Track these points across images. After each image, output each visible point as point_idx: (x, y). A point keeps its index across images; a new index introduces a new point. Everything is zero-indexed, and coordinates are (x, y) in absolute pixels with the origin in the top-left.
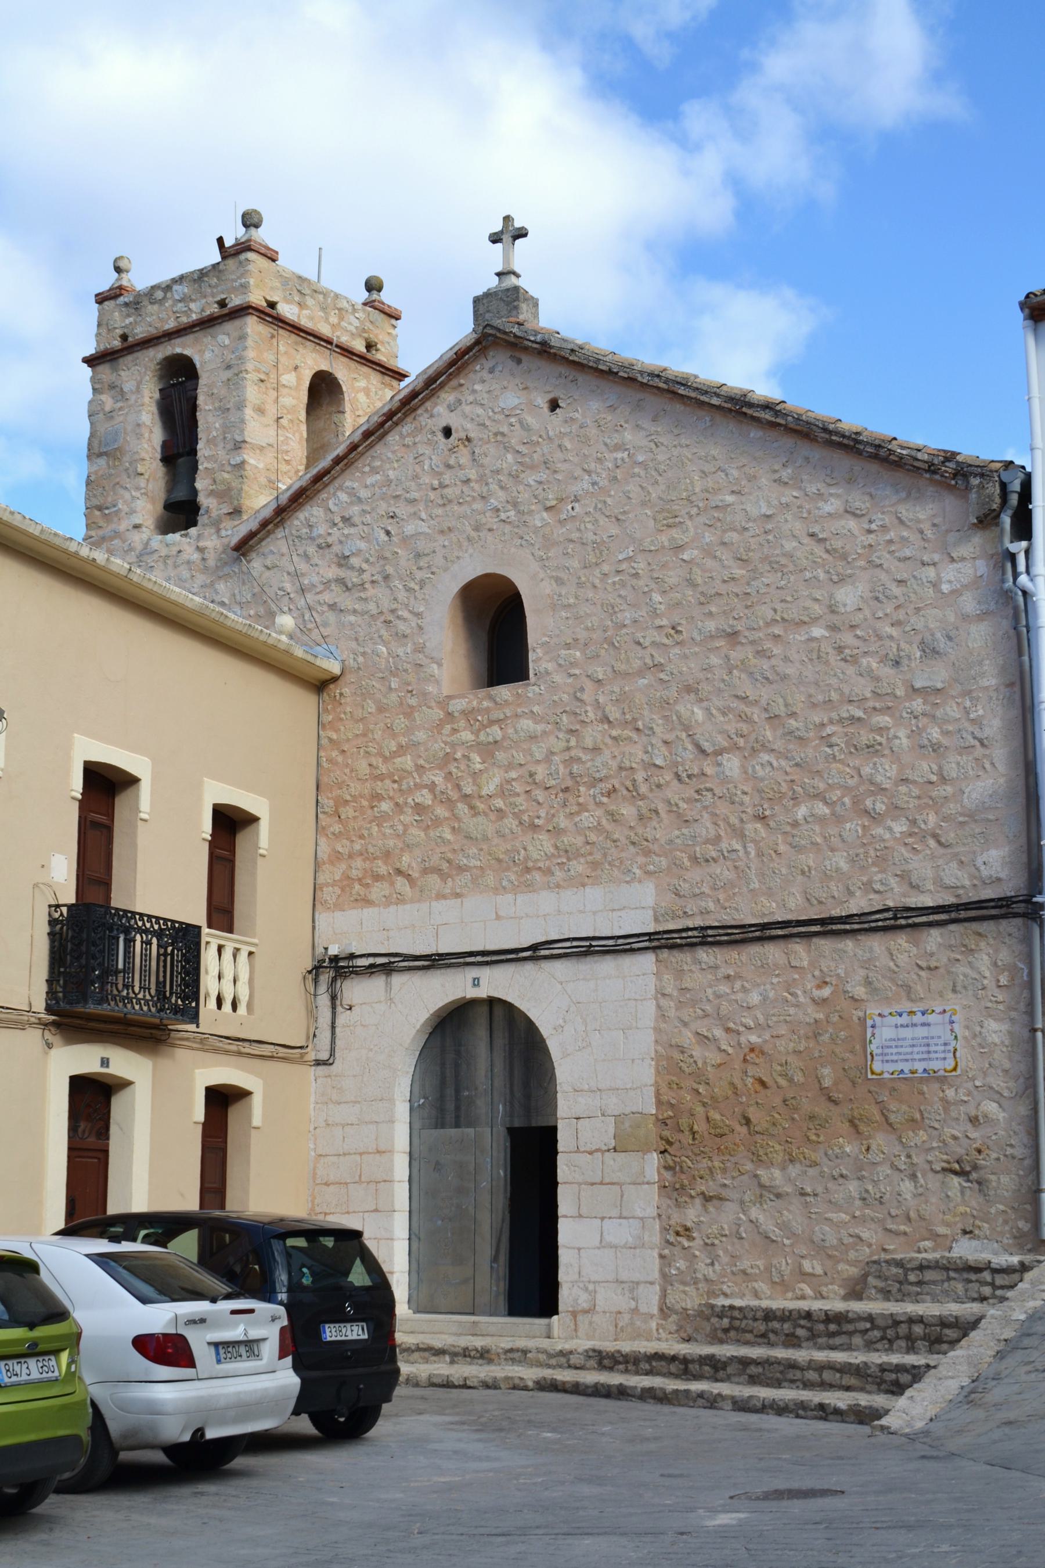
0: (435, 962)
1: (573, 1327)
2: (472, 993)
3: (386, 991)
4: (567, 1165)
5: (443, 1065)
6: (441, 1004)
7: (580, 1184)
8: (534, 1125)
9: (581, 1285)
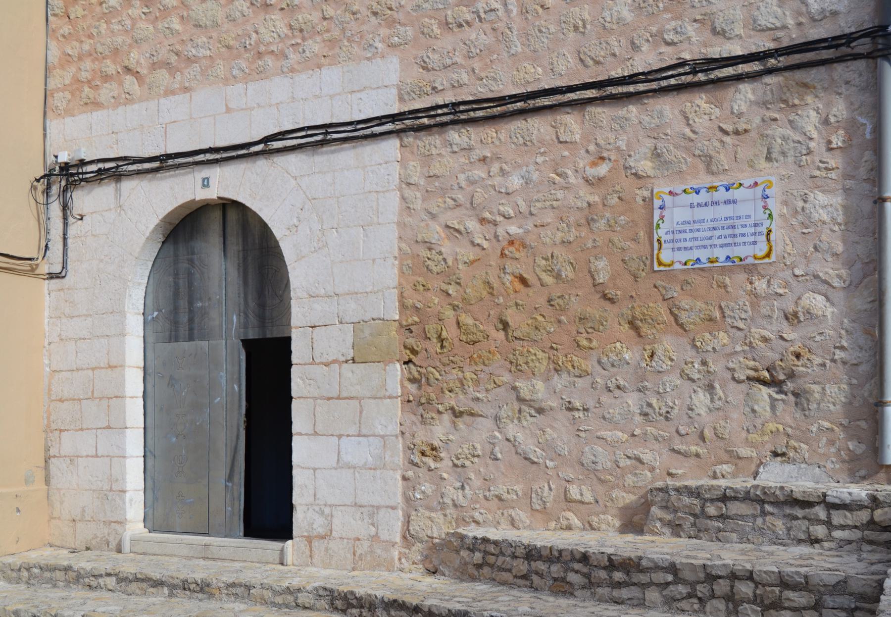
0: (164, 163)
1: (308, 553)
3: (116, 197)
5: (176, 275)
7: (315, 399)
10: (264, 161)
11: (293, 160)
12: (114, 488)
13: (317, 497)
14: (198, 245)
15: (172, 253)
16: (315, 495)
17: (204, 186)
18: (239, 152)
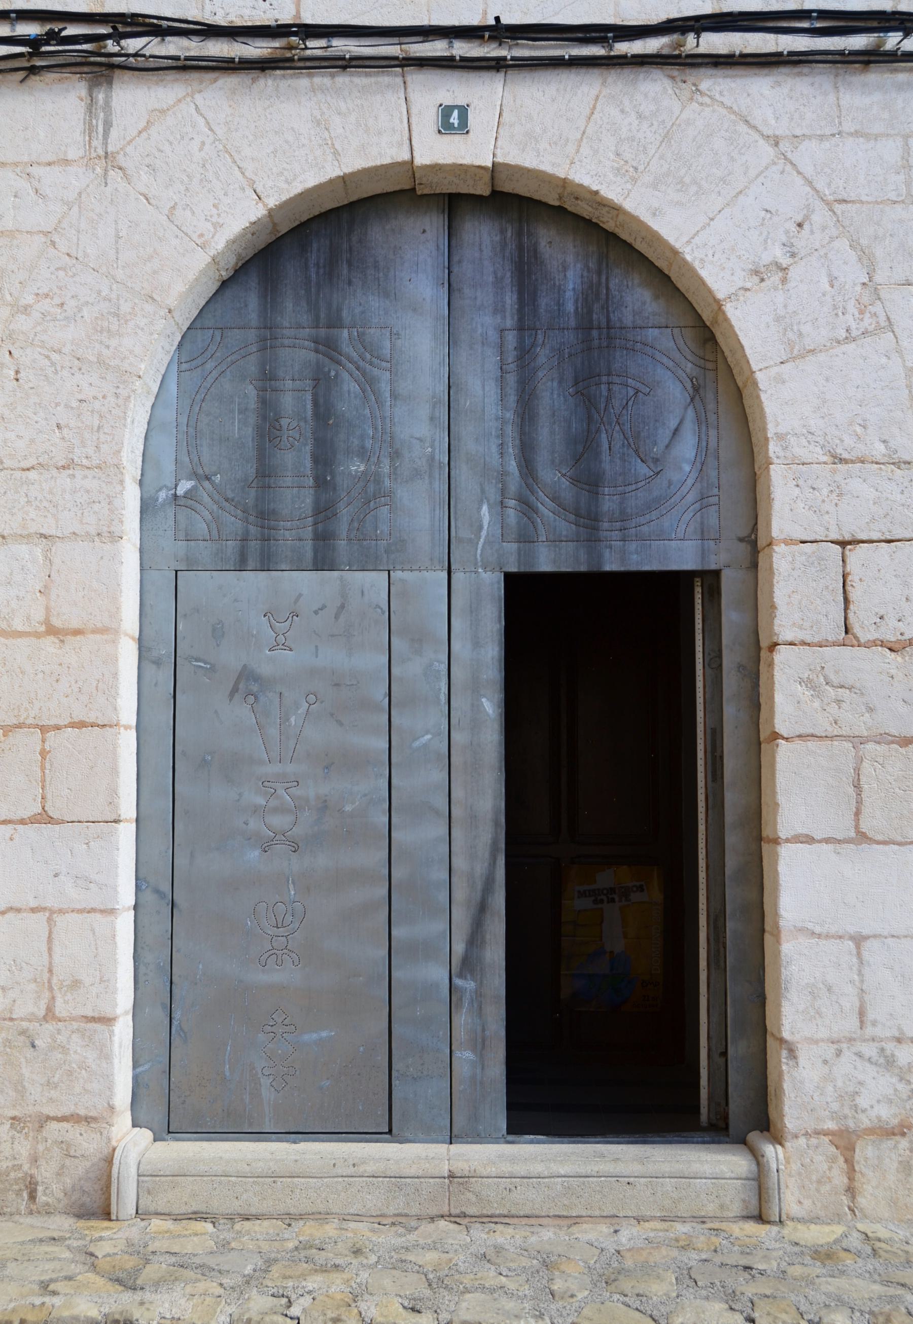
0: (291, 50)
1: (840, 1180)
2: (434, 150)
3: (90, 130)
4: (808, 683)
5: (268, 379)
6: (311, 180)
7: (858, 741)
8: (611, 564)
9: (870, 1050)
10: (667, 83)
11: (766, 91)
12: (61, 1009)
13: (871, 1015)
14: (360, 302)
15: (253, 317)
16: (862, 1014)
17: (445, 127)
18: (596, 47)
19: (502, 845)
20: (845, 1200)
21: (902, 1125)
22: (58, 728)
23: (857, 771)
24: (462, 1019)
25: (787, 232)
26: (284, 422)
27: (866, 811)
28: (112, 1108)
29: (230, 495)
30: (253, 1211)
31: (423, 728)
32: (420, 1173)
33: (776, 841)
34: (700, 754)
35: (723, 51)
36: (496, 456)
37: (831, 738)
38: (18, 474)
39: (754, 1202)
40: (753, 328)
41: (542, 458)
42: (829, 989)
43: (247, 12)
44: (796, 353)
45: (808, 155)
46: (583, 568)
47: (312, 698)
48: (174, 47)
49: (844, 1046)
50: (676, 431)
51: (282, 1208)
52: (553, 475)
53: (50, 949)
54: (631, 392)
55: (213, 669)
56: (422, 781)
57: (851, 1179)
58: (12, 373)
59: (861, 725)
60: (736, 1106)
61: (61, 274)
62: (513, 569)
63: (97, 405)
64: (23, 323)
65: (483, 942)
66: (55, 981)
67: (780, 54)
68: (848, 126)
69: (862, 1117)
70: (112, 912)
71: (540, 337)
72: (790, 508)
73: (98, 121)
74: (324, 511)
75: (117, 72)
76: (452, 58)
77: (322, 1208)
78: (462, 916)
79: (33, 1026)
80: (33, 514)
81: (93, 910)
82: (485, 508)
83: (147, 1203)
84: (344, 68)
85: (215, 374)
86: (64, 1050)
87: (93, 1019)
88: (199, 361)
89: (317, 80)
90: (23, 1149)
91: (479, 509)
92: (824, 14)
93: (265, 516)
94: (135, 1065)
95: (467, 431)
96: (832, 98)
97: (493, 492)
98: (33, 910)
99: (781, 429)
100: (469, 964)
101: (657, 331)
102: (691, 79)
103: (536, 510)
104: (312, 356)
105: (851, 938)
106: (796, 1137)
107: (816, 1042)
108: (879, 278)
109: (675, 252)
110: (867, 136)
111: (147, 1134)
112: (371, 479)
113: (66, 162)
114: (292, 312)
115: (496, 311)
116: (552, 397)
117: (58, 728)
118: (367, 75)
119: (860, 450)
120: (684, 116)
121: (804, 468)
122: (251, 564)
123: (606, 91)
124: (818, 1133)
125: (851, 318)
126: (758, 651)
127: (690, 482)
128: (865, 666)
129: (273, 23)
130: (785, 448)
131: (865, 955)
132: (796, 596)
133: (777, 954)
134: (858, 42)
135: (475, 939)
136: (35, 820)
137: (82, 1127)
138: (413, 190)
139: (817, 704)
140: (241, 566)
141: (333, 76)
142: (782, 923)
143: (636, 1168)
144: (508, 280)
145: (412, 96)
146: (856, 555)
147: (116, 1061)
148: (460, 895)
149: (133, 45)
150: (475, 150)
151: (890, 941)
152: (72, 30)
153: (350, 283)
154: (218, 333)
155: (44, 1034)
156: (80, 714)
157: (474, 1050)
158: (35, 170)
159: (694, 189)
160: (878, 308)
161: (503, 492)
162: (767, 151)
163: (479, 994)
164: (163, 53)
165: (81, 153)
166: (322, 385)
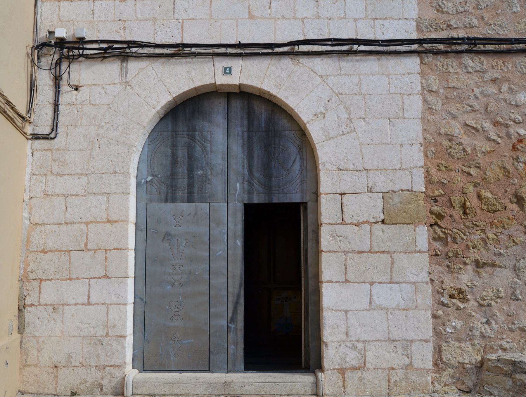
0: (180, 51)
1: (341, 383)
2: (222, 80)
3: (121, 75)
4: (331, 235)
5: (174, 147)
6: (186, 89)
7: (346, 252)
8: (275, 201)
10: (290, 60)
11: (319, 62)
12: (110, 333)
13: (350, 334)
14: (202, 124)
15: (170, 128)
16: (347, 333)
17: (225, 73)
19: (243, 284)
20: (342, 389)
21: (359, 367)
22: (110, 250)
23: (346, 261)
24: (231, 336)
25: (325, 103)
26: (179, 159)
27: (348, 273)
28: (125, 363)
29: (163, 181)
30: (167, 393)
31: (220, 250)
32: (216, 382)
33: (322, 282)
34: (302, 257)
35: (306, 50)
36: (241, 169)
37: (338, 252)
38: (99, 175)
39: (315, 390)
40: (314, 131)
41: (255, 170)
42: (338, 326)
43: (167, 40)
44: (328, 138)
45: (331, 81)
46: (267, 202)
47: (187, 241)
48: (146, 50)
49: (342, 343)
50: (294, 161)
51: (175, 392)
52: (257, 174)
53: (107, 316)
54: (281, 150)
55: (158, 232)
56: (219, 265)
57: (344, 383)
58: (98, 146)
59: (347, 248)
60: (312, 362)
61: (113, 116)
62: (246, 202)
63: (123, 155)
64: (101, 131)
65: (237, 313)
66: (109, 325)
67: (323, 51)
68: (343, 72)
69: (347, 364)
70: (125, 304)
71: (254, 134)
72: (326, 184)
73: (124, 72)
74: (191, 185)
75: (130, 58)
76: (227, 53)
77: (187, 392)
78: (231, 306)
79: (102, 339)
80: (103, 187)
81: (120, 304)
82: (238, 184)
83: (135, 391)
84: (195, 56)
85: (159, 145)
86: (111, 346)
87: (120, 336)
88: (154, 142)
89: (188, 60)
90: (99, 375)
91: (236, 184)
92: (335, 40)
93: (173, 187)
94: (134, 350)
95: (233, 162)
96: (338, 64)
97: (240, 180)
98: (102, 304)
99: (323, 161)
100: (233, 320)
101: (288, 132)
102: (297, 59)
103: (253, 185)
104: (187, 140)
105: (344, 311)
106: (328, 370)
107: (334, 342)
108: (351, 116)
109: (292, 109)
110: (348, 75)
111: (137, 371)
112: (204, 176)
113: (114, 84)
114: (181, 127)
115: (241, 127)
116: (257, 151)
117: (110, 250)
118: (202, 58)
119: (346, 167)
120: (295, 70)
121: (330, 172)
122: (169, 201)
123: (272, 62)
124: (334, 369)
125: (343, 128)
126: (318, 225)
127: (298, 176)
128: (349, 230)
129: (175, 43)
130: (324, 166)
131: (348, 316)
132: (328, 209)
133: (322, 315)
134: (345, 48)
135: (235, 312)
136: (103, 277)
137: (116, 369)
138: (217, 91)
139: (334, 242)
140: (166, 201)
141: (192, 58)
142: (323, 307)
143: (280, 380)
144: (245, 117)
145: (215, 64)
146: (345, 198)
147: (127, 349)
148: (230, 299)
149: (134, 50)
150: (234, 80)
151: (355, 312)
152: (116, 46)
153: (198, 118)
154: (160, 133)
155: (105, 341)
156: (116, 246)
157: (234, 345)
158: (106, 87)
159: (297, 91)
160: (351, 125)
161: (243, 179)
162: (319, 79)
163: (236, 329)
164: (143, 52)
165: (119, 81)
166: (190, 148)
